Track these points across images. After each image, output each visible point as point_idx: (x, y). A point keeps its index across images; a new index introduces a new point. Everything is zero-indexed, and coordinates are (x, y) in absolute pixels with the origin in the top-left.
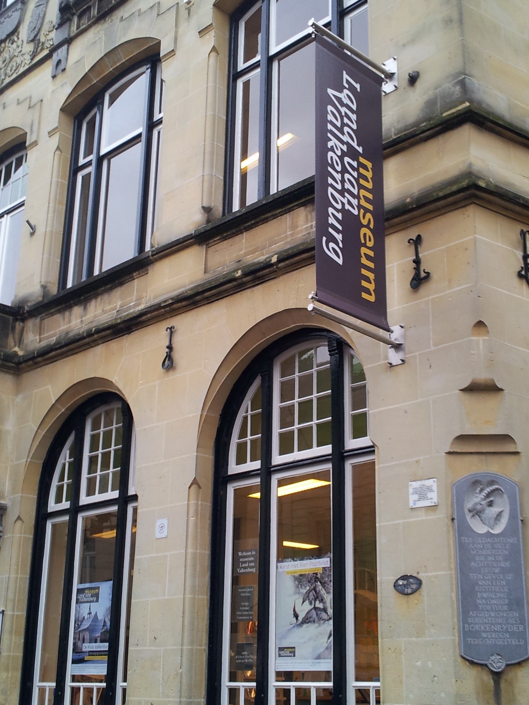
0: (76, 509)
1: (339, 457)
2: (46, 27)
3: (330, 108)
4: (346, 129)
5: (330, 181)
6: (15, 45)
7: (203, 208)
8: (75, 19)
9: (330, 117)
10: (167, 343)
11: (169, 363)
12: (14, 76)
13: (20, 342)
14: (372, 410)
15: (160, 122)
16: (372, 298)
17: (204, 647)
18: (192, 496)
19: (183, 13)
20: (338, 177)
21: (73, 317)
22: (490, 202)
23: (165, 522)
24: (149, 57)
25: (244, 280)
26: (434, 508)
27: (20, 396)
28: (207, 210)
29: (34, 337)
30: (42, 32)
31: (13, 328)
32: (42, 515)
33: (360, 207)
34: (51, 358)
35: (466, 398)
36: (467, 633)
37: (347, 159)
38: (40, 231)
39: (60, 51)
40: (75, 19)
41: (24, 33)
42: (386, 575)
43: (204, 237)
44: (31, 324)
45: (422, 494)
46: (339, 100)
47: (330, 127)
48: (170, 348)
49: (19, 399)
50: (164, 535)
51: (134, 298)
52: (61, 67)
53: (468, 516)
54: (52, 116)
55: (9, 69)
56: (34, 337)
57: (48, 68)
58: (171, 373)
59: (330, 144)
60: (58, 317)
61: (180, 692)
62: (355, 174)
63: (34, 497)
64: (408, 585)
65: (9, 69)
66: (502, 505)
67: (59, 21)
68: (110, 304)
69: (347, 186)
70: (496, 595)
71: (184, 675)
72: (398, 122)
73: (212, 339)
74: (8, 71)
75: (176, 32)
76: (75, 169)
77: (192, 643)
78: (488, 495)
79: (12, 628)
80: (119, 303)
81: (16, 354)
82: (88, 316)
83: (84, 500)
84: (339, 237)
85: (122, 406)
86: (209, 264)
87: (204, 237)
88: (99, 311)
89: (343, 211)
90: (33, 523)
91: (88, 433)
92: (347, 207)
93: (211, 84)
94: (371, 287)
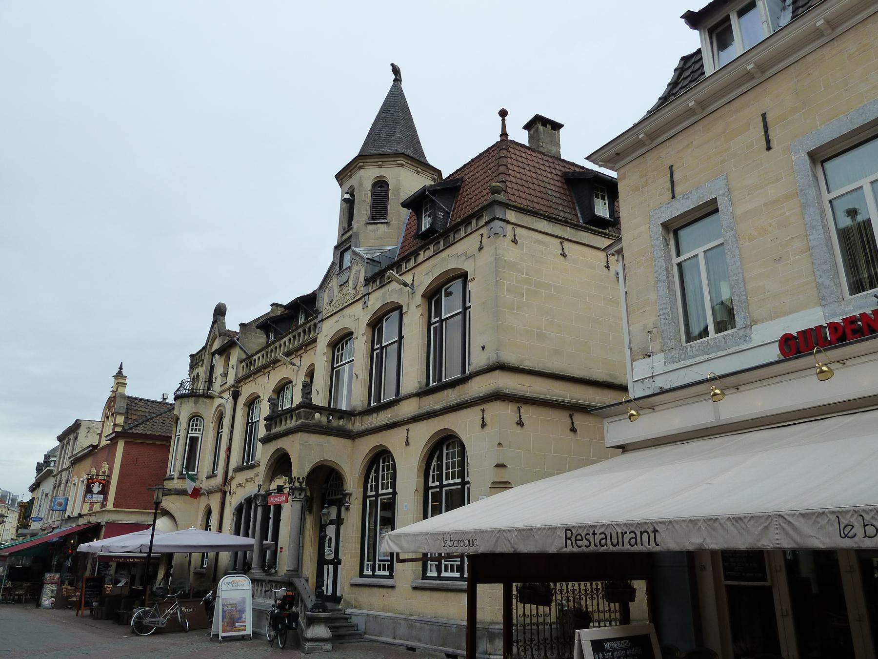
0: (441, 486)
11: (407, 444)
13: (353, 425)
15: (470, 307)
28: (420, 382)
29: (358, 425)
32: (365, 497)
35: (496, 469)
38: (360, 377)
41: (350, 282)
43: (419, 394)
44: (358, 418)
56: (358, 425)
57: (360, 305)
73: (422, 434)
83: (380, 492)
87: (419, 394)
91: (381, 465)
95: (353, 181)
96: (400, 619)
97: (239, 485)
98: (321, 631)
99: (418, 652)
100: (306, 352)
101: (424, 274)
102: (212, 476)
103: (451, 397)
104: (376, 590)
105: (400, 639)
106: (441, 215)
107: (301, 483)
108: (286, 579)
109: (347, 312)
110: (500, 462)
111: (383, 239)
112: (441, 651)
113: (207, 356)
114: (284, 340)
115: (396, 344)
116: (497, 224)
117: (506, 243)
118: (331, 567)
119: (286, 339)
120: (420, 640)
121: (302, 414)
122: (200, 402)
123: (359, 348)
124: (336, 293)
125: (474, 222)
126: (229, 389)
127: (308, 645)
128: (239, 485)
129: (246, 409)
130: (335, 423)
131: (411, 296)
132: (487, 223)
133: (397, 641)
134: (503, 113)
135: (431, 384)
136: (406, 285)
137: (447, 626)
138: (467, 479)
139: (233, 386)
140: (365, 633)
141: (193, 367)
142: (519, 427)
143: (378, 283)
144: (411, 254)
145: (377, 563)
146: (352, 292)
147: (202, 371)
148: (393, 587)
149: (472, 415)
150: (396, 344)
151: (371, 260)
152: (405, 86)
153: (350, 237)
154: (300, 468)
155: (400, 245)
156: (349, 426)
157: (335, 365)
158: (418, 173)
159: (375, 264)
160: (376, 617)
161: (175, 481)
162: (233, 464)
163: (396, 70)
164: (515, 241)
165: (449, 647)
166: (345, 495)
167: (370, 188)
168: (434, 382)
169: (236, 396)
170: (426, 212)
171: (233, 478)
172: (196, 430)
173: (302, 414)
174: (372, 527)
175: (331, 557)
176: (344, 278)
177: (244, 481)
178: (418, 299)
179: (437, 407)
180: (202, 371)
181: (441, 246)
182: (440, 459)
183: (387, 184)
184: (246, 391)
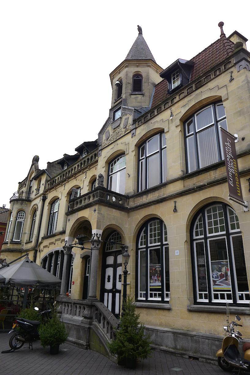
0: (147, 247)
3: (226, 147)
4: (230, 152)
5: (229, 166)
6: (119, 129)
7: (182, 171)
8: (137, 123)
9: (226, 150)
10: (174, 205)
11: (175, 210)
12: (120, 137)
13: (128, 205)
14: (168, 236)
16: (240, 195)
18: (186, 245)
19: (170, 122)
20: (230, 164)
21: (144, 198)
23: (178, 251)
24: (161, 132)
25: (197, 189)
27: (130, 218)
28: (182, 171)
29: (132, 204)
30: (127, 126)
31: (126, 201)
32: (137, 249)
33: (235, 171)
34: (138, 209)
37: (231, 160)
38: (132, 176)
39: (133, 131)
40: (137, 123)
41: (122, 126)
44: (131, 200)
46: (227, 145)
47: (227, 152)
48: (175, 206)
49: (129, 219)
50: (178, 254)
51: (162, 193)
52: (134, 135)
54: (132, 147)
55: (118, 135)
57: (130, 136)
58: (176, 213)
59: (227, 156)
61: (187, 294)
62: (233, 163)
65: (118, 135)
67: (132, 123)
68: (155, 195)
69: (232, 167)
70: (120, 265)
71: (188, 290)
72: (240, 150)
73: (187, 205)
74: (118, 136)
75: (169, 126)
76: (139, 160)
77: (189, 282)
79: (132, 277)
80: (157, 195)
81: (127, 207)
82: (148, 198)
83: (149, 245)
84: (232, 179)
85: (160, 221)
86: (185, 185)
88: (152, 197)
89: (232, 173)
90: (135, 251)
92: (232, 172)
94: (239, 192)
95: (122, 75)
97: (45, 247)
101: (180, 108)
102: (29, 242)
104: (153, 311)
111: (143, 101)
113: (28, 182)
114: (74, 166)
118: (110, 294)
122: (24, 204)
124: (111, 133)
126: (40, 196)
128: (45, 247)
129: (91, 185)
132: (235, 64)
134: (221, 25)
138: (164, 243)
139: (43, 194)
141: (20, 188)
145: (149, 292)
147: (24, 189)
150: (159, 154)
152: (144, 35)
159: (139, 113)
161: (9, 245)
162: (42, 235)
163: (140, 29)
167: (132, 77)
169: (44, 200)
170: (174, 79)
171: (41, 243)
172: (21, 218)
176: (117, 124)
177: (48, 244)
180: (24, 189)
182: (146, 232)
183: (141, 76)
184: (50, 196)
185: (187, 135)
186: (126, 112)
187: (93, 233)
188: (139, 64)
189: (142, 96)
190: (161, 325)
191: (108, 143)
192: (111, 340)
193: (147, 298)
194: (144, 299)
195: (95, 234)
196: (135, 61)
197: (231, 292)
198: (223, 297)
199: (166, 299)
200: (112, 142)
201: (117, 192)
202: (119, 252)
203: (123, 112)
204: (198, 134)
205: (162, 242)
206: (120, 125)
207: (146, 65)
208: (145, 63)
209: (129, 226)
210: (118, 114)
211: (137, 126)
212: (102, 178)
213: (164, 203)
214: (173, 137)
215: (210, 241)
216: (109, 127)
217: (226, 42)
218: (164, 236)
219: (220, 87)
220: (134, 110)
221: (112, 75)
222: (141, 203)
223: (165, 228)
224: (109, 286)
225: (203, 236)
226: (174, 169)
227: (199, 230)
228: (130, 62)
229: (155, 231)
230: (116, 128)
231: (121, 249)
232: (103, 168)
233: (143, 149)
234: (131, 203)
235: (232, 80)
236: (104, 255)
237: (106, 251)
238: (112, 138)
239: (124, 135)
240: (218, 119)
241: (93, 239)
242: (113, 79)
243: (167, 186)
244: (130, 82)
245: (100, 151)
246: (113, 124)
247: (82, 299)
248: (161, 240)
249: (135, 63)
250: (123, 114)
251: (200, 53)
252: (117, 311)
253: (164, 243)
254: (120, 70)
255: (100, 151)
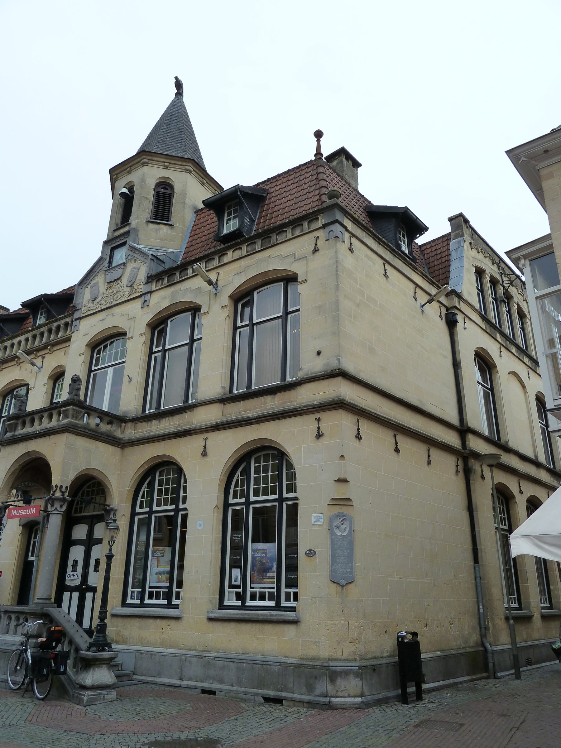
0: (151, 513)
1: (177, 510)
2: (137, 282)
7: (222, 387)
11: (204, 454)
13: (123, 432)
14: (188, 495)
17: (219, 575)
18: (96, 703)
22: (347, 408)
23: (202, 522)
26: (321, 525)
29: (130, 432)
30: (135, 284)
32: (133, 514)
35: (336, 484)
36: (333, 572)
41: (125, 280)
42: (302, 549)
43: (223, 401)
44: (129, 424)
45: (317, 519)
48: (205, 447)
52: (146, 304)
53: (335, 528)
56: (130, 432)
57: (138, 303)
60: (144, 424)
63: (130, 505)
64: (311, 553)
66: (346, 525)
67: (146, 281)
70: (100, 541)
78: (342, 521)
83: (155, 508)
88: (167, 424)
93: (226, 332)
95: (135, 177)
96: (191, 656)
98: (101, 675)
99: (219, 695)
100: (51, 352)
101: (235, 272)
103: (271, 404)
104: (151, 622)
105: (190, 679)
106: (247, 220)
107: (63, 493)
108: (38, 610)
109: (116, 310)
110: (342, 476)
111: (168, 241)
112: (257, 694)
115: (281, 321)
116: (337, 228)
117: (343, 248)
118: (76, 595)
119: (22, 338)
120: (221, 682)
121: (71, 412)
123: (136, 349)
125: (178, 274)
127: (87, 695)
129: (51, 383)
130: (105, 428)
131: (213, 296)
132: (324, 226)
133: (185, 683)
134: (319, 135)
135: (148, 411)
136: (210, 282)
137: (264, 664)
138: (181, 506)
140: (134, 674)
142: (357, 440)
143: (165, 281)
144: (215, 253)
145: (147, 590)
146: (128, 289)
148: (178, 618)
149: (305, 425)
150: (187, 347)
151: (156, 257)
152: (186, 99)
153: (128, 233)
154: (62, 476)
155: (183, 250)
156: (118, 433)
157: (93, 368)
158: (203, 184)
159: (159, 262)
160: (151, 654)
163: (179, 85)
164: (351, 249)
165: (268, 689)
166: (108, 512)
168: (150, 409)
170: (229, 214)
173: (71, 412)
174: (142, 548)
175: (77, 582)
178: (225, 299)
179: (251, 414)
181: (258, 246)
182: (151, 485)
183: (171, 187)
185: (239, 324)
186: (135, 255)
187: (53, 484)
188: (169, 163)
189: (169, 227)
190: (163, 644)
191: (94, 307)
192: (75, 670)
193: (142, 599)
194: (138, 602)
195: (56, 486)
196: (163, 156)
197: (275, 590)
198: (262, 598)
199: (175, 602)
200: (104, 307)
201: (105, 408)
202: (100, 518)
203: (130, 253)
204: (255, 327)
205: (177, 505)
206: (123, 278)
207: (183, 167)
208: (181, 163)
209: (119, 472)
210: (120, 255)
211: (154, 288)
212: (78, 383)
213: (187, 439)
214: (215, 324)
215: (253, 508)
216: (99, 277)
217: (321, 171)
218: (181, 495)
219: (297, 257)
220: (150, 257)
221: (114, 171)
222: (147, 434)
223: (185, 482)
224: (73, 579)
225: (243, 500)
226: (211, 378)
227: (239, 488)
228: (152, 156)
229: (167, 483)
230: (114, 281)
231: (103, 512)
232: (81, 355)
233: (163, 332)
234: (130, 431)
235: (315, 251)
236: (69, 522)
237: (73, 515)
238: (103, 301)
239: (126, 299)
240: (289, 310)
241: (53, 495)
242: (116, 179)
243: (195, 409)
244: (148, 197)
245: (76, 319)
246: (107, 273)
247: (16, 603)
248: (175, 501)
249: (164, 160)
250: (130, 257)
251: (279, 175)
252: (86, 624)
253: (181, 506)
254: (130, 167)
255: (76, 319)
